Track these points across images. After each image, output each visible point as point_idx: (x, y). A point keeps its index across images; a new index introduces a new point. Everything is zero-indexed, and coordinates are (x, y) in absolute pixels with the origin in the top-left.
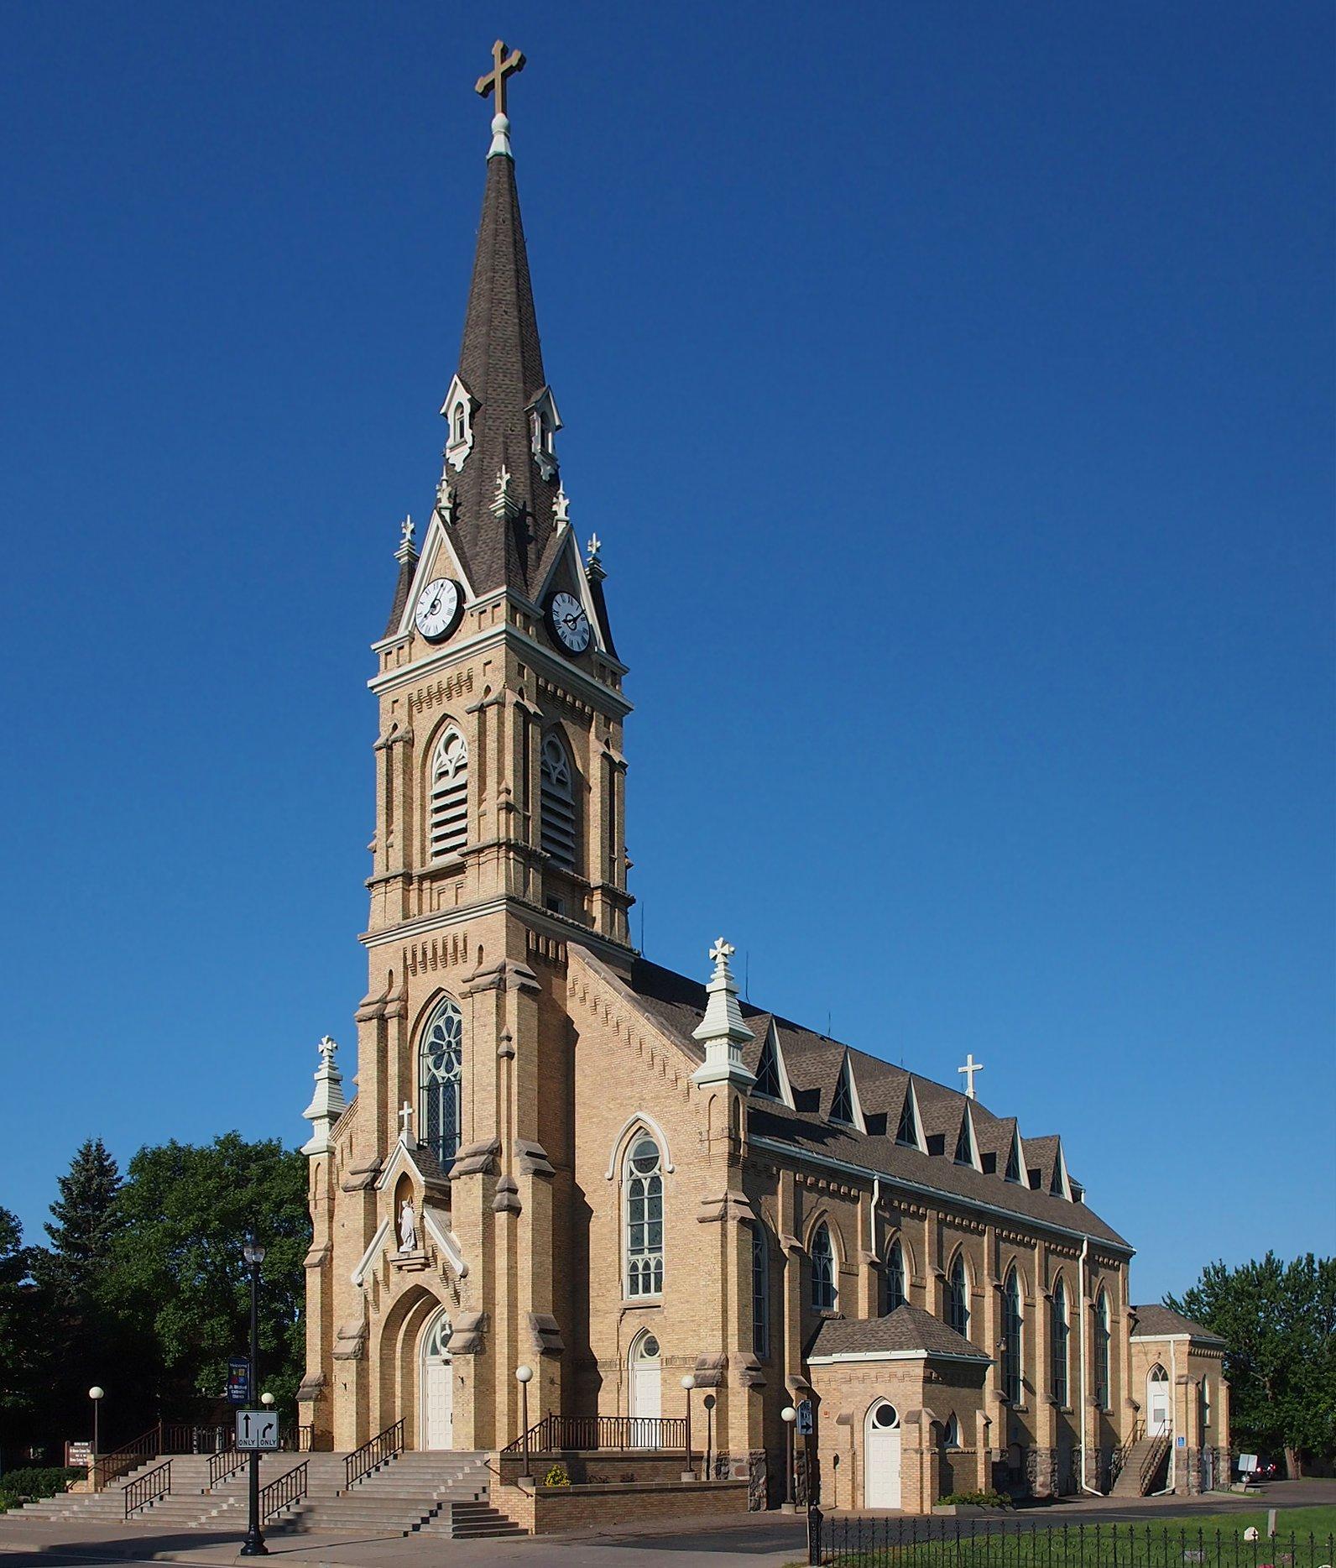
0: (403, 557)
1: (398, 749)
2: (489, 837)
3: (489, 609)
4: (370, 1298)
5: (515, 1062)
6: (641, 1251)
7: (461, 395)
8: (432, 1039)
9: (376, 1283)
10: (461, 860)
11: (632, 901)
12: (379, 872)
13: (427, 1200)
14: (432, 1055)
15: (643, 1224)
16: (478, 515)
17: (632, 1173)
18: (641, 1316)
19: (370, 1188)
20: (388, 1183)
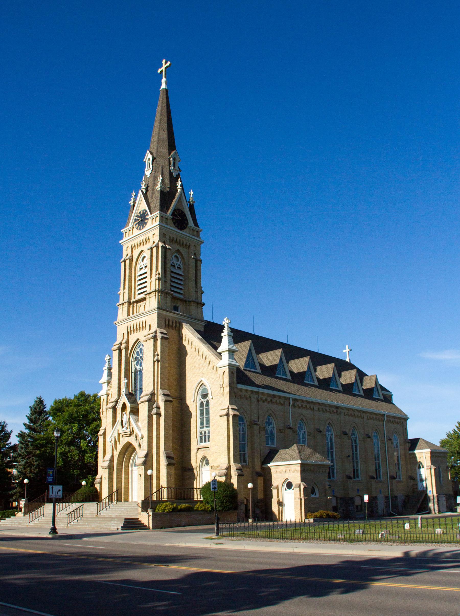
0: (132, 203)
1: (128, 262)
2: (153, 289)
3: (155, 218)
4: (114, 446)
5: (160, 363)
6: (203, 427)
7: (150, 156)
8: (136, 356)
9: (115, 441)
10: (145, 296)
11: (204, 305)
12: (121, 301)
13: (131, 412)
14: (136, 361)
15: (204, 418)
16: (153, 190)
17: (200, 399)
18: (203, 451)
19: (114, 409)
20: (119, 407)
